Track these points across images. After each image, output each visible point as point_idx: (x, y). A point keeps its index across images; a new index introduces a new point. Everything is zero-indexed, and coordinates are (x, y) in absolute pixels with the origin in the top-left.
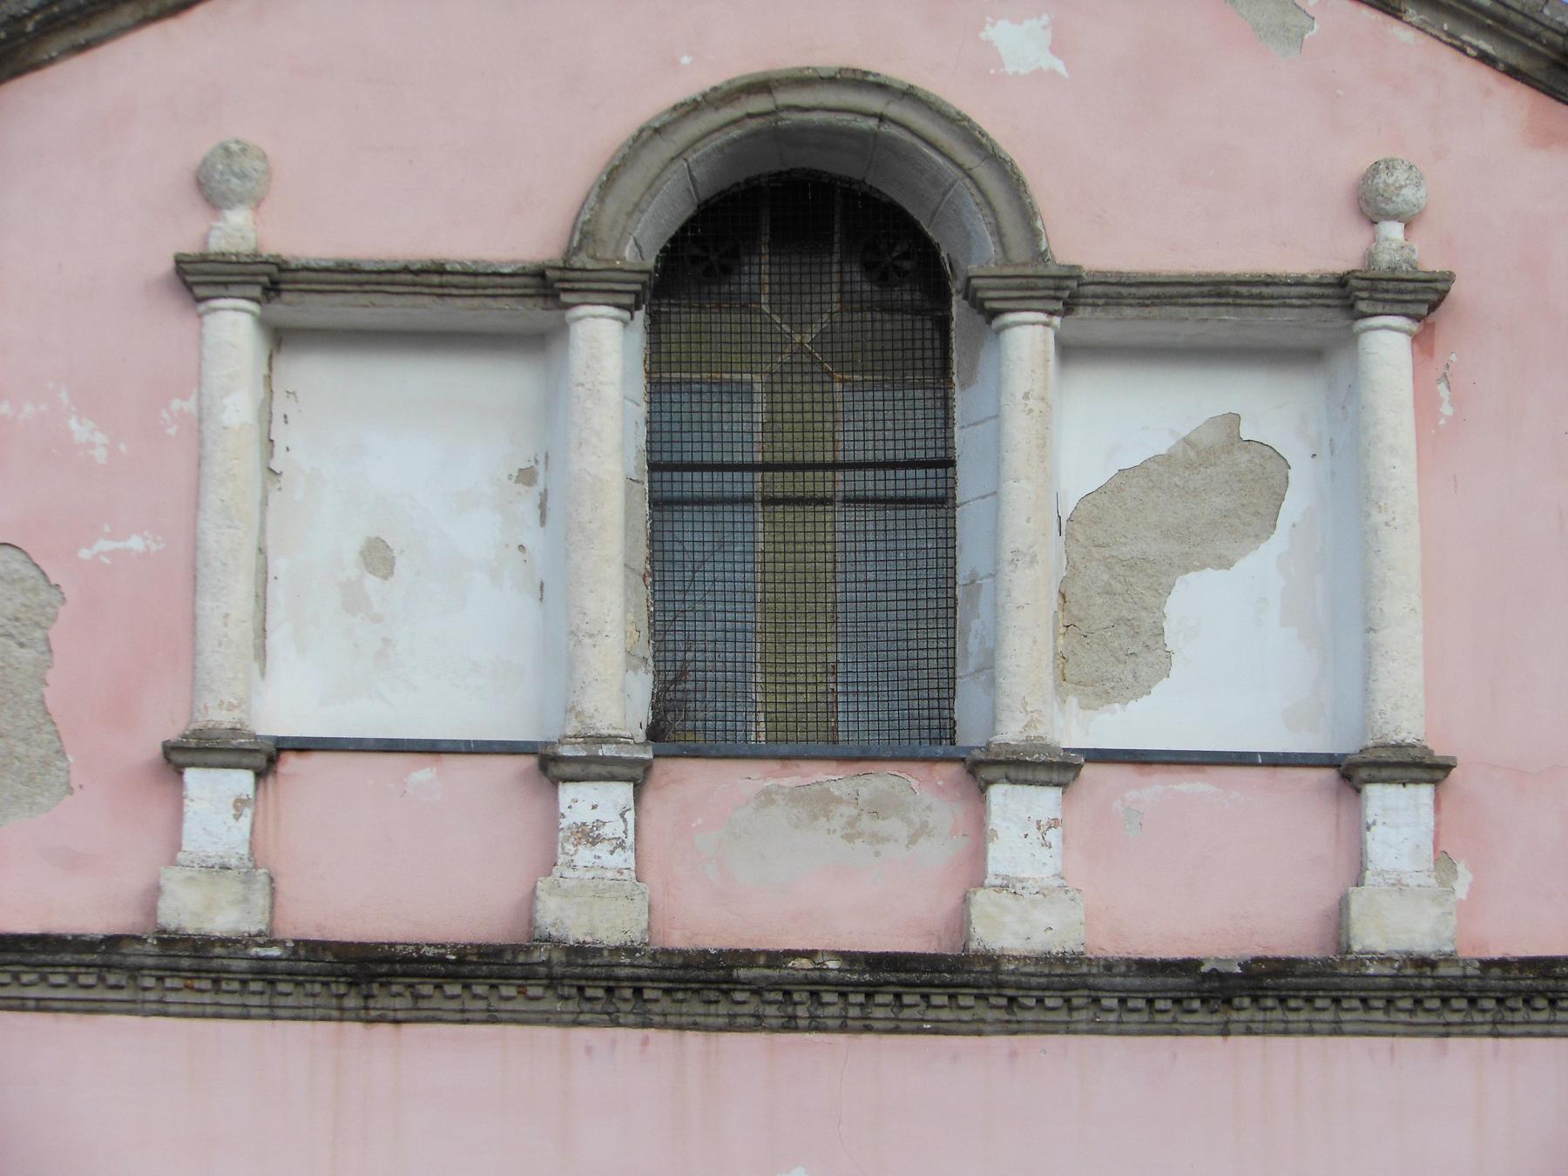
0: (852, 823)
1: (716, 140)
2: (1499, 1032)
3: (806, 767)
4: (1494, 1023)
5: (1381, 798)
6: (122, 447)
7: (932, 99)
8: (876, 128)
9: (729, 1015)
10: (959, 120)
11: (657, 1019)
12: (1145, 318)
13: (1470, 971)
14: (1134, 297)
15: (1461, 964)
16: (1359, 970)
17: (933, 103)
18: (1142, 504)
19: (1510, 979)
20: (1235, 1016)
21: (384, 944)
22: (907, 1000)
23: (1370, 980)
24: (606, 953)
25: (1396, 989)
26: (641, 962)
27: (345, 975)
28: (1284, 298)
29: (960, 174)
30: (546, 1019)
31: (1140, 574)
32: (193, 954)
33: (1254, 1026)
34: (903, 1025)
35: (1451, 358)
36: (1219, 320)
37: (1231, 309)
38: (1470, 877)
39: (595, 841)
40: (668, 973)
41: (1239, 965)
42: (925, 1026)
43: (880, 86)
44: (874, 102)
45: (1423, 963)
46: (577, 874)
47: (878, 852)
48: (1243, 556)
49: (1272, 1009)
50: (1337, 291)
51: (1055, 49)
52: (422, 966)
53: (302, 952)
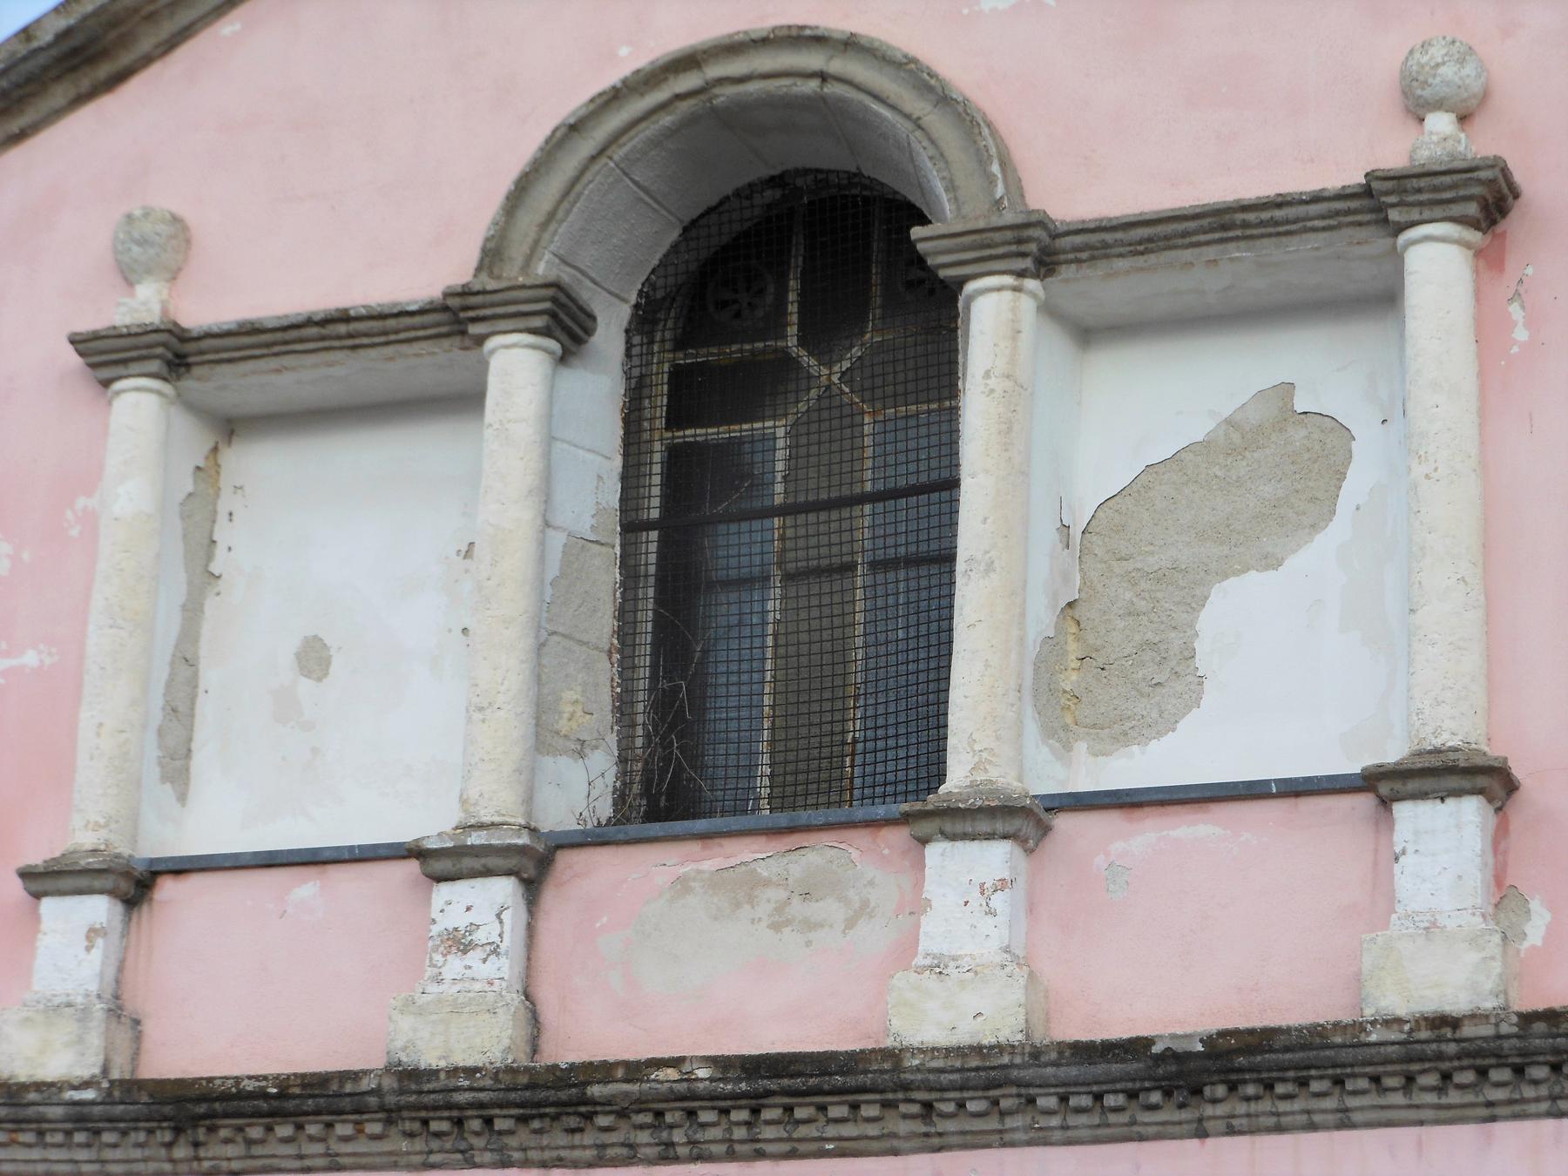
0: (780, 908)
1: (644, 130)
2: (1560, 1110)
3: (730, 845)
4: (1554, 1098)
6: (26, 556)
7: (876, 44)
8: (819, 90)
9: (597, 1146)
10: (906, 64)
11: (516, 1155)
12: (1142, 269)
13: (1505, 1029)
14: (1122, 244)
15: (1493, 1020)
16: (1358, 1037)
17: (877, 49)
18: (1175, 503)
19: (1559, 1036)
20: (1209, 1110)
21: (202, 1079)
22: (800, 1113)
23: (1373, 1051)
24: (442, 1075)
25: (1410, 1060)
26: (481, 1084)
27: (166, 1119)
28: (1304, 220)
29: (909, 125)
31: (1170, 587)
32: (8, 1101)
33: (1235, 1122)
34: (802, 1147)
35: (1526, 272)
36: (1231, 260)
37: (1242, 244)
38: (1548, 916)
39: (465, 948)
40: (513, 1096)
41: (1201, 1041)
42: (827, 1147)
44: (812, 60)
45: (1443, 1022)
46: (441, 988)
47: (810, 942)
48: (1294, 551)
49: (1257, 1098)
50: (1365, 202)
52: (242, 1104)
53: (117, 1094)
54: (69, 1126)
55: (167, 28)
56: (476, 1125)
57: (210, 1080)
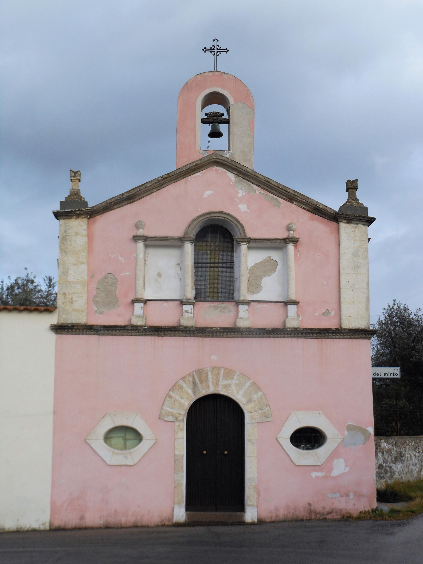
0: (221, 310)
3: (215, 303)
5: (290, 307)
11: (196, 336)
13: (301, 330)
14: (257, 241)
20: (271, 335)
24: (189, 327)
30: (181, 336)
39: (188, 313)
43: (225, 213)
44: (224, 216)
45: (295, 329)
51: (247, 208)
54: (143, 330)
55: (140, 197)
56: (192, 332)
57: (161, 326)
